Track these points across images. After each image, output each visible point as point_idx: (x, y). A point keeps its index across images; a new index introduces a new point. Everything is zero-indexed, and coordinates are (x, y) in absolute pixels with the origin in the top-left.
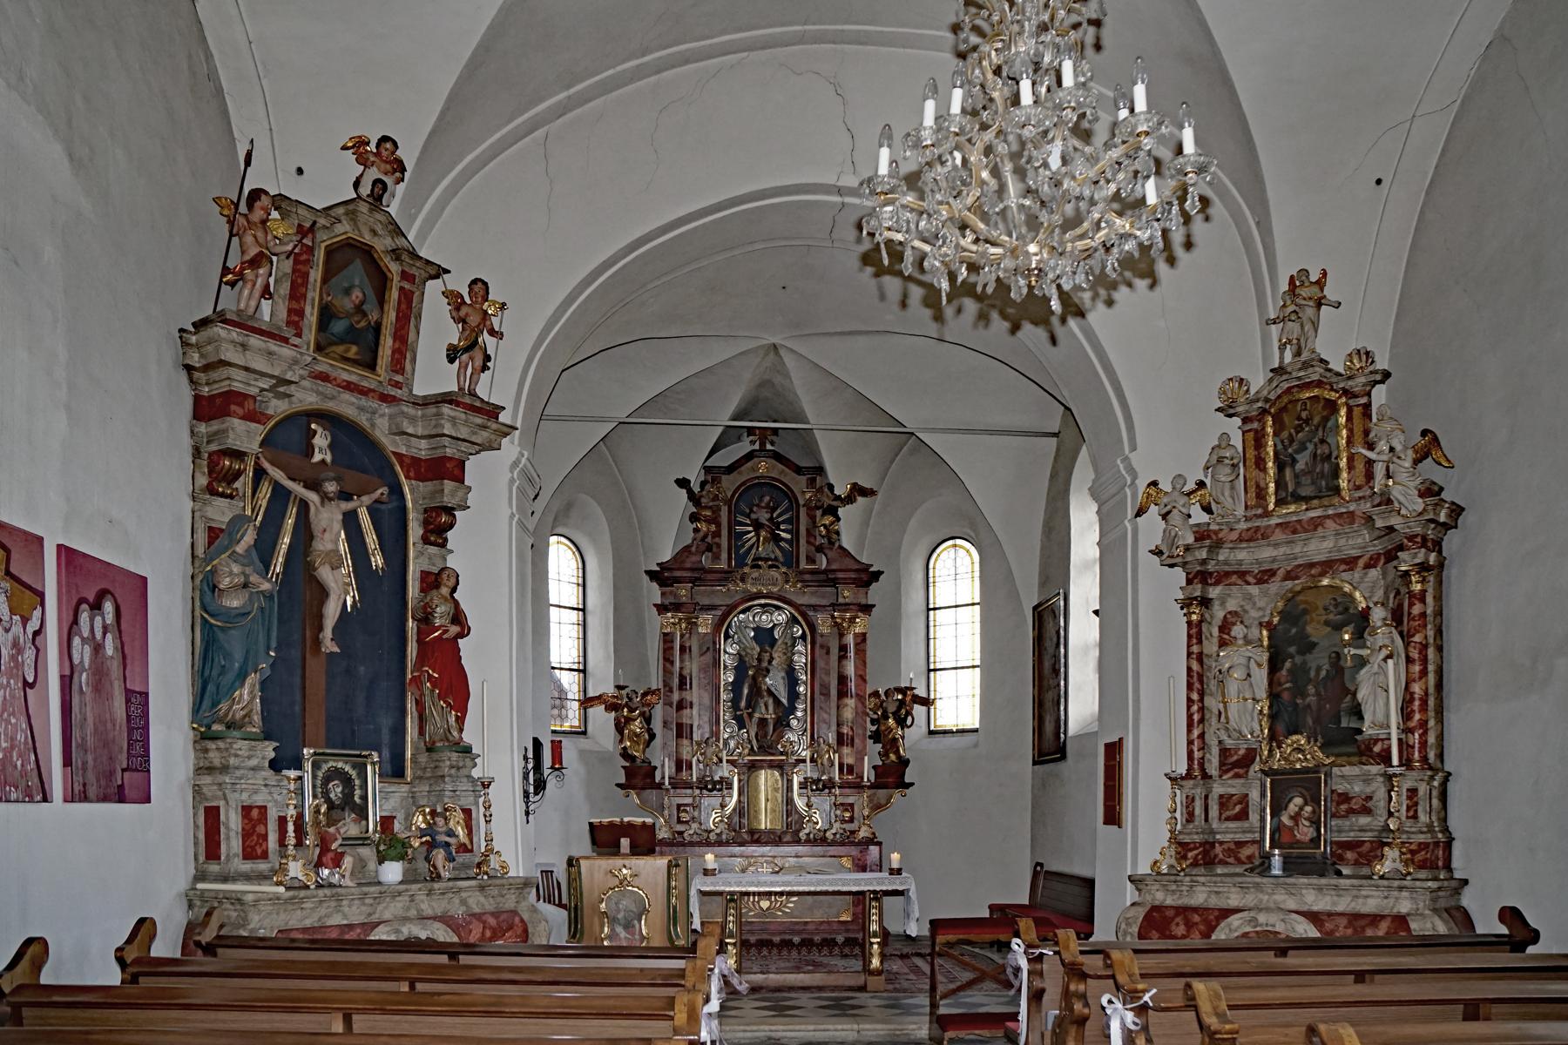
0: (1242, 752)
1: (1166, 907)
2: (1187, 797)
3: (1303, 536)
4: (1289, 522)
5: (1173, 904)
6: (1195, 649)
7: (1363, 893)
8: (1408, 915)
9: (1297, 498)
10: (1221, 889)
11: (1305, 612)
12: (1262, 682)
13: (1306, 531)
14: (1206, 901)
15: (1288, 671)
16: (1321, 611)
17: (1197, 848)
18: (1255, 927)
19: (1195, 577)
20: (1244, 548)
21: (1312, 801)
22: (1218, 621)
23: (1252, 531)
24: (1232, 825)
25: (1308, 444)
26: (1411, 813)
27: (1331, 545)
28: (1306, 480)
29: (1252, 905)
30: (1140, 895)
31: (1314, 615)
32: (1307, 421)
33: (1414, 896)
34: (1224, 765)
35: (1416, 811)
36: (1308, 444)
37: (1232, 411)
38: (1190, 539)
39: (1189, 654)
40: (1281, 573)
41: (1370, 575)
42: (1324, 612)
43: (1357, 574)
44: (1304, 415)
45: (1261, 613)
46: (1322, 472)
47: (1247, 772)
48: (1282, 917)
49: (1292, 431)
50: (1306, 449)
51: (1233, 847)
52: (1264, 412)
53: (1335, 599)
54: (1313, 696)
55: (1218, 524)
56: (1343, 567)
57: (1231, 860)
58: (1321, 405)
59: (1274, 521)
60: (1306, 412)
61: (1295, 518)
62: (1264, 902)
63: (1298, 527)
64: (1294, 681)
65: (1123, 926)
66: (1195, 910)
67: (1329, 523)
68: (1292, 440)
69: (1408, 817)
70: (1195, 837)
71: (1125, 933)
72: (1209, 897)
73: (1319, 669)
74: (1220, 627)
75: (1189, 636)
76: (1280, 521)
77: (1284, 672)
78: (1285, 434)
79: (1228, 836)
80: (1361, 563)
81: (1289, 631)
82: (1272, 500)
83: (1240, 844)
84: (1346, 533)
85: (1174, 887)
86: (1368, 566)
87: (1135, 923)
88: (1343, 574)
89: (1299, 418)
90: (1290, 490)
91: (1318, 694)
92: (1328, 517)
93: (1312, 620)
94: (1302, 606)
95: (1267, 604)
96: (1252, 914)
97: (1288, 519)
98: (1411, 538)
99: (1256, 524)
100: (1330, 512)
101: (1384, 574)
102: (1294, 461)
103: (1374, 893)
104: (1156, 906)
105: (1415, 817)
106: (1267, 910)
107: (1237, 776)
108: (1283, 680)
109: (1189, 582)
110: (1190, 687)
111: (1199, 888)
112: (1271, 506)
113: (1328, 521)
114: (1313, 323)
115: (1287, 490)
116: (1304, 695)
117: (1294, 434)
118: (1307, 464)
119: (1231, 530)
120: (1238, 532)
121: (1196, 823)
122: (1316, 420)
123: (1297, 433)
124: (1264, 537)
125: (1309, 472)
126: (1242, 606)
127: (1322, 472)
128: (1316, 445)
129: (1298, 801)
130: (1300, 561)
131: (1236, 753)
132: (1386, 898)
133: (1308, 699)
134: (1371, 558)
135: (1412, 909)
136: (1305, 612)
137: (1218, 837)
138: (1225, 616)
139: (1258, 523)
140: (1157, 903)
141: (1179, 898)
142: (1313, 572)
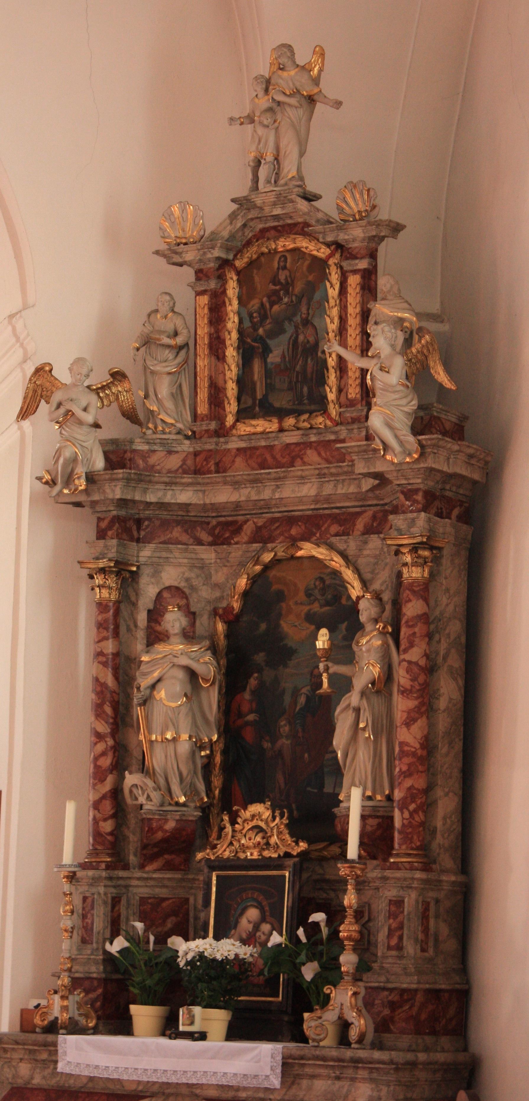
1: (33, 1090)
2: (85, 899)
4: (256, 448)
7: (308, 1070)
13: (279, 465)
15: (253, 693)
16: (301, 596)
17: (94, 990)
19: (110, 527)
21: (272, 915)
23: (202, 456)
26: (394, 942)
27: (313, 492)
31: (291, 603)
33: (375, 1075)
35: (401, 938)
36: (286, 324)
37: (177, 259)
38: (99, 463)
40: (248, 529)
41: (371, 545)
44: (282, 276)
45: (218, 594)
49: (265, 299)
52: (224, 264)
53: (322, 580)
54: (287, 737)
56: (335, 528)
58: (307, 263)
59: (234, 444)
60: (286, 272)
61: (263, 443)
67: (311, 455)
68: (264, 317)
69: (389, 948)
73: (296, 693)
74: (149, 611)
76: (243, 445)
77: (247, 695)
80: (360, 524)
84: (332, 475)
89: (275, 281)
90: (259, 396)
92: (309, 445)
97: (254, 444)
98: (409, 494)
99: (208, 447)
100: (313, 438)
102: (267, 350)
103: (322, 1071)
104: (18, 1088)
105: (399, 947)
107: (168, 867)
112: (230, 420)
113: (309, 452)
114: (297, 133)
115: (254, 399)
117: (268, 306)
118: (283, 356)
119: (170, 452)
120: (182, 456)
122: (299, 287)
123: (272, 304)
124: (220, 469)
126: (187, 580)
128: (296, 327)
129: (253, 913)
132: (338, 1078)
133: (279, 743)
138: (159, 594)
140: (20, 1082)
142: (294, 532)
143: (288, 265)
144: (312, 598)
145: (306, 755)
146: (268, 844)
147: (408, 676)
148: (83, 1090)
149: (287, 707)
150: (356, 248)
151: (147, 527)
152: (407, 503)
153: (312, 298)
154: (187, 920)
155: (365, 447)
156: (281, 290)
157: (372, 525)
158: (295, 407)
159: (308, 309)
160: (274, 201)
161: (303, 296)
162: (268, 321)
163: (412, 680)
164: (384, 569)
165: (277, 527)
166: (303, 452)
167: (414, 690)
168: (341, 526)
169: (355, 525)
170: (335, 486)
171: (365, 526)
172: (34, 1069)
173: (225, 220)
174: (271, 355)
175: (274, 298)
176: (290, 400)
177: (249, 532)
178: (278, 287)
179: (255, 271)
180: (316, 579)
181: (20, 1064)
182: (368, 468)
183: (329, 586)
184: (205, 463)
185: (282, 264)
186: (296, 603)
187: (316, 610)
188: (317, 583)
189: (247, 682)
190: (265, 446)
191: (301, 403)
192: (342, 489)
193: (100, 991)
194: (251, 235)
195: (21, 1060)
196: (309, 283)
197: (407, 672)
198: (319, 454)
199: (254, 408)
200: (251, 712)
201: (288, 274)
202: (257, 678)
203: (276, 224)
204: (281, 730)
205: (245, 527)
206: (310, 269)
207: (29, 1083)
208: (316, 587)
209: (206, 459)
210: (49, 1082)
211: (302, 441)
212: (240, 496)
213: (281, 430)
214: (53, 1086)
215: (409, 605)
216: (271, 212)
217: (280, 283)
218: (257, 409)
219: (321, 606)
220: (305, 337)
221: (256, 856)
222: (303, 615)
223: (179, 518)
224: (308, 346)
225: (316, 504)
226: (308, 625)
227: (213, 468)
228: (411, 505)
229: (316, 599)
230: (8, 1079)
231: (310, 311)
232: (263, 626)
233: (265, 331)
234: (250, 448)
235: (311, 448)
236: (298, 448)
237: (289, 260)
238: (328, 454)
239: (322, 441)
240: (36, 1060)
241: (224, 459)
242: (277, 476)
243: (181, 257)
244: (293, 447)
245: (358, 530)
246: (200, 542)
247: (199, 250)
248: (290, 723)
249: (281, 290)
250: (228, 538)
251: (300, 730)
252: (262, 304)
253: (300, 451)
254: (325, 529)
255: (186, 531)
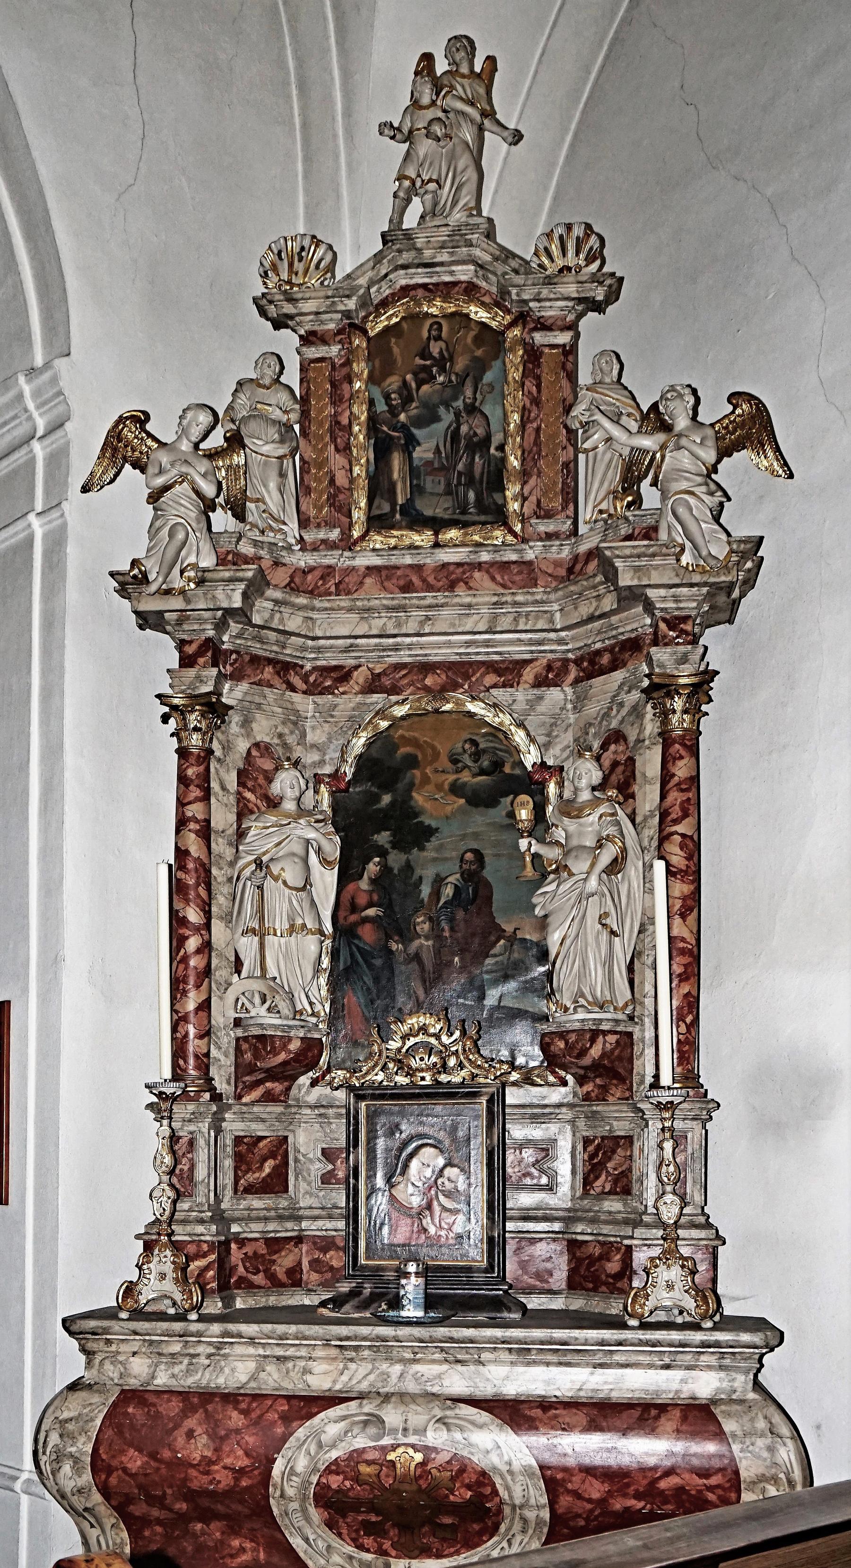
0: (295, 1045)
1: (158, 1393)
3: (430, 598)
4: (397, 568)
5: (174, 1385)
6: (195, 810)
8: (714, 1401)
9: (417, 522)
10: (291, 1352)
11: (412, 762)
12: (327, 897)
14: (253, 1378)
15: (373, 881)
16: (444, 762)
17: (205, 1255)
18: (379, 1437)
20: (301, 608)
22: (237, 758)
23: (317, 573)
24: (257, 1203)
25: (442, 410)
28: (433, 484)
29: (364, 1386)
30: (89, 1364)
32: (442, 363)
34: (251, 1069)
36: (442, 410)
39: (181, 823)
40: (360, 677)
42: (449, 766)
43: (521, 695)
44: (435, 348)
46: (469, 471)
47: (289, 1089)
48: (439, 1413)
49: (409, 377)
50: (436, 419)
51: (263, 1250)
54: (427, 938)
55: (256, 543)
56: (491, 679)
57: (259, 1279)
58: (472, 334)
59: (364, 560)
60: (442, 344)
61: (408, 560)
62: (394, 1379)
63: (415, 579)
64: (388, 906)
65: (54, 1439)
66: (231, 1398)
70: (200, 1229)
71: (59, 1457)
72: (261, 1369)
73: (439, 882)
74: (241, 773)
75: (183, 779)
76: (376, 561)
77: (364, 884)
78: (393, 382)
79: (255, 1226)
80: (528, 675)
81: (377, 798)
82: (359, 515)
83: (275, 1244)
85: (176, 1348)
86: (541, 682)
87: (84, 1431)
88: (494, 692)
89: (424, 353)
91: (436, 934)
92: (479, 566)
93: (426, 780)
94: (403, 750)
95: (330, 739)
96: (368, 1407)
97: (394, 560)
99: (327, 561)
100: (485, 557)
101: (579, 703)
102: (411, 442)
106: (403, 1397)
107: (269, 1098)
108: (362, 900)
109: (187, 661)
110: (177, 889)
111: (239, 1350)
113: (477, 575)
115: (394, 503)
116: (406, 934)
117: (414, 385)
118: (437, 451)
121: (199, 1200)
122: (461, 364)
125: (442, 468)
126: (280, 736)
127: (469, 471)
128: (457, 415)
130: (404, 657)
131: (284, 1047)
133: (416, 943)
134: (549, 667)
135: (718, 1390)
136: (412, 762)
137: (235, 1228)
138: (249, 752)
139: (330, 558)
140: (133, 1383)
141: (188, 1372)
143: (444, 334)
144: (460, 765)
145: (456, 959)
146: (444, 1065)
147: (682, 854)
148: (242, 1391)
149: (426, 900)
150: (551, 317)
151: (236, 660)
152: (671, 633)
153: (481, 379)
154: (286, 1164)
155: (643, 549)
156: (433, 366)
157: (547, 676)
158: (455, 517)
159: (475, 393)
160: (444, 241)
161: (468, 375)
162: (414, 405)
163: (687, 859)
164: (566, 730)
165: (404, 676)
166: (468, 574)
167: (690, 871)
168: (500, 676)
169: (521, 676)
170: (515, 619)
171: (536, 677)
172: (156, 1366)
173: (369, 260)
174: (418, 449)
175: (422, 375)
176: (448, 508)
177: (361, 681)
178: (428, 363)
179: (393, 340)
180: (466, 741)
181: (132, 1359)
182: (639, 579)
183: (484, 751)
184: (321, 582)
185: (434, 333)
186: (436, 771)
187: (466, 779)
188: (467, 746)
189: (364, 869)
190: (410, 566)
191: (464, 512)
192: (526, 624)
193: (213, 1257)
194: (388, 292)
195: (134, 1354)
196: (475, 359)
197: (682, 849)
198: (493, 579)
199: (394, 516)
200: (370, 905)
201: (443, 345)
202: (379, 863)
203: (427, 280)
204: (418, 928)
205: (355, 673)
206: (478, 341)
207: (148, 1384)
208: (465, 751)
209: (322, 578)
210: (182, 1382)
211: (468, 560)
212: (370, 628)
213: (437, 545)
214: (189, 1387)
215: (680, 763)
216: (435, 257)
217: (431, 356)
218: (398, 516)
219: (475, 775)
220: (471, 428)
221: (428, 1081)
222: (446, 787)
223: (272, 656)
224: (475, 439)
225: (468, 647)
226: (454, 798)
227: (333, 589)
228: (677, 637)
229: (466, 767)
230: (112, 1379)
231: (478, 396)
232: (386, 799)
233: (408, 417)
234: (386, 568)
235: (479, 570)
236: (461, 570)
237: (445, 329)
238: (506, 578)
239: (497, 562)
240: (160, 1354)
241: (346, 579)
242: (435, 601)
243: (296, 308)
244: (452, 568)
245: (526, 682)
246: (293, 689)
247: (328, 297)
248: (431, 919)
249: (433, 366)
250: (329, 686)
251: (446, 928)
252: (405, 382)
253: (464, 573)
254: (477, 680)
255: (278, 673)
